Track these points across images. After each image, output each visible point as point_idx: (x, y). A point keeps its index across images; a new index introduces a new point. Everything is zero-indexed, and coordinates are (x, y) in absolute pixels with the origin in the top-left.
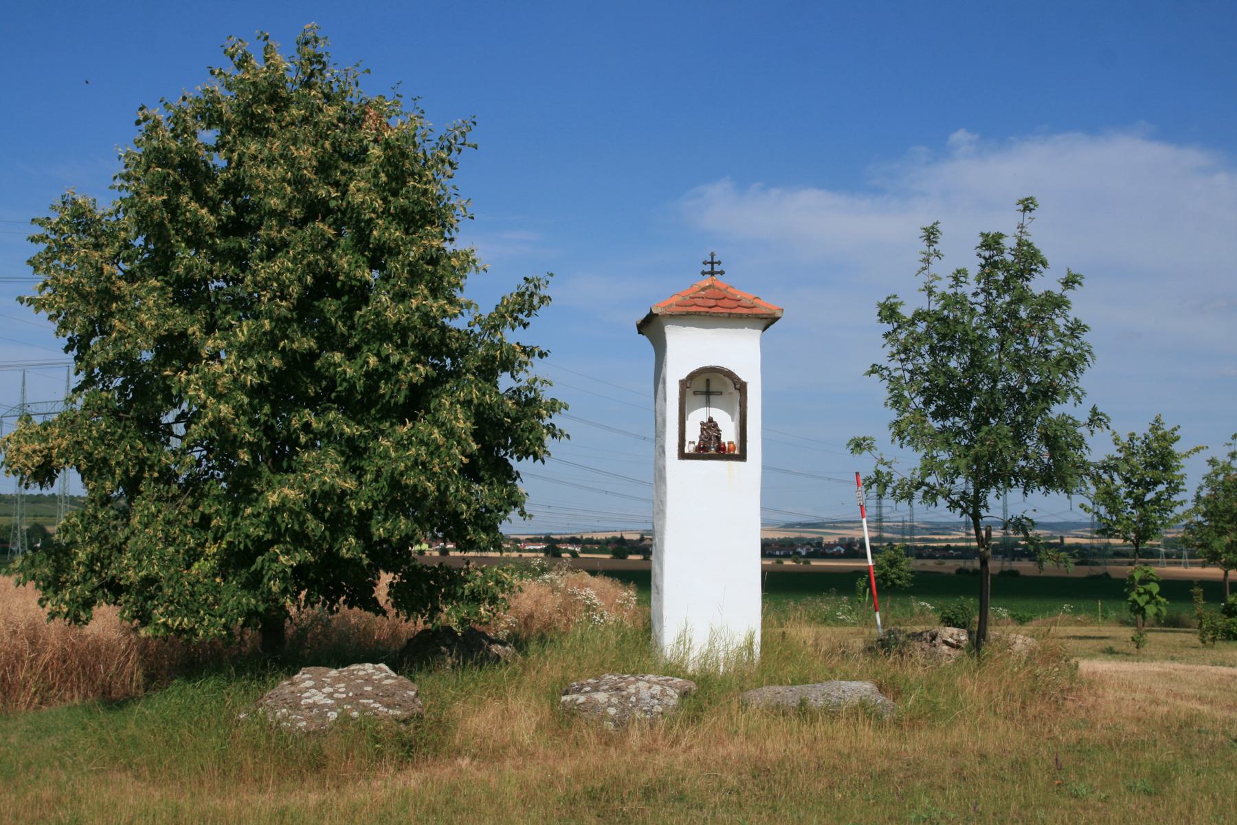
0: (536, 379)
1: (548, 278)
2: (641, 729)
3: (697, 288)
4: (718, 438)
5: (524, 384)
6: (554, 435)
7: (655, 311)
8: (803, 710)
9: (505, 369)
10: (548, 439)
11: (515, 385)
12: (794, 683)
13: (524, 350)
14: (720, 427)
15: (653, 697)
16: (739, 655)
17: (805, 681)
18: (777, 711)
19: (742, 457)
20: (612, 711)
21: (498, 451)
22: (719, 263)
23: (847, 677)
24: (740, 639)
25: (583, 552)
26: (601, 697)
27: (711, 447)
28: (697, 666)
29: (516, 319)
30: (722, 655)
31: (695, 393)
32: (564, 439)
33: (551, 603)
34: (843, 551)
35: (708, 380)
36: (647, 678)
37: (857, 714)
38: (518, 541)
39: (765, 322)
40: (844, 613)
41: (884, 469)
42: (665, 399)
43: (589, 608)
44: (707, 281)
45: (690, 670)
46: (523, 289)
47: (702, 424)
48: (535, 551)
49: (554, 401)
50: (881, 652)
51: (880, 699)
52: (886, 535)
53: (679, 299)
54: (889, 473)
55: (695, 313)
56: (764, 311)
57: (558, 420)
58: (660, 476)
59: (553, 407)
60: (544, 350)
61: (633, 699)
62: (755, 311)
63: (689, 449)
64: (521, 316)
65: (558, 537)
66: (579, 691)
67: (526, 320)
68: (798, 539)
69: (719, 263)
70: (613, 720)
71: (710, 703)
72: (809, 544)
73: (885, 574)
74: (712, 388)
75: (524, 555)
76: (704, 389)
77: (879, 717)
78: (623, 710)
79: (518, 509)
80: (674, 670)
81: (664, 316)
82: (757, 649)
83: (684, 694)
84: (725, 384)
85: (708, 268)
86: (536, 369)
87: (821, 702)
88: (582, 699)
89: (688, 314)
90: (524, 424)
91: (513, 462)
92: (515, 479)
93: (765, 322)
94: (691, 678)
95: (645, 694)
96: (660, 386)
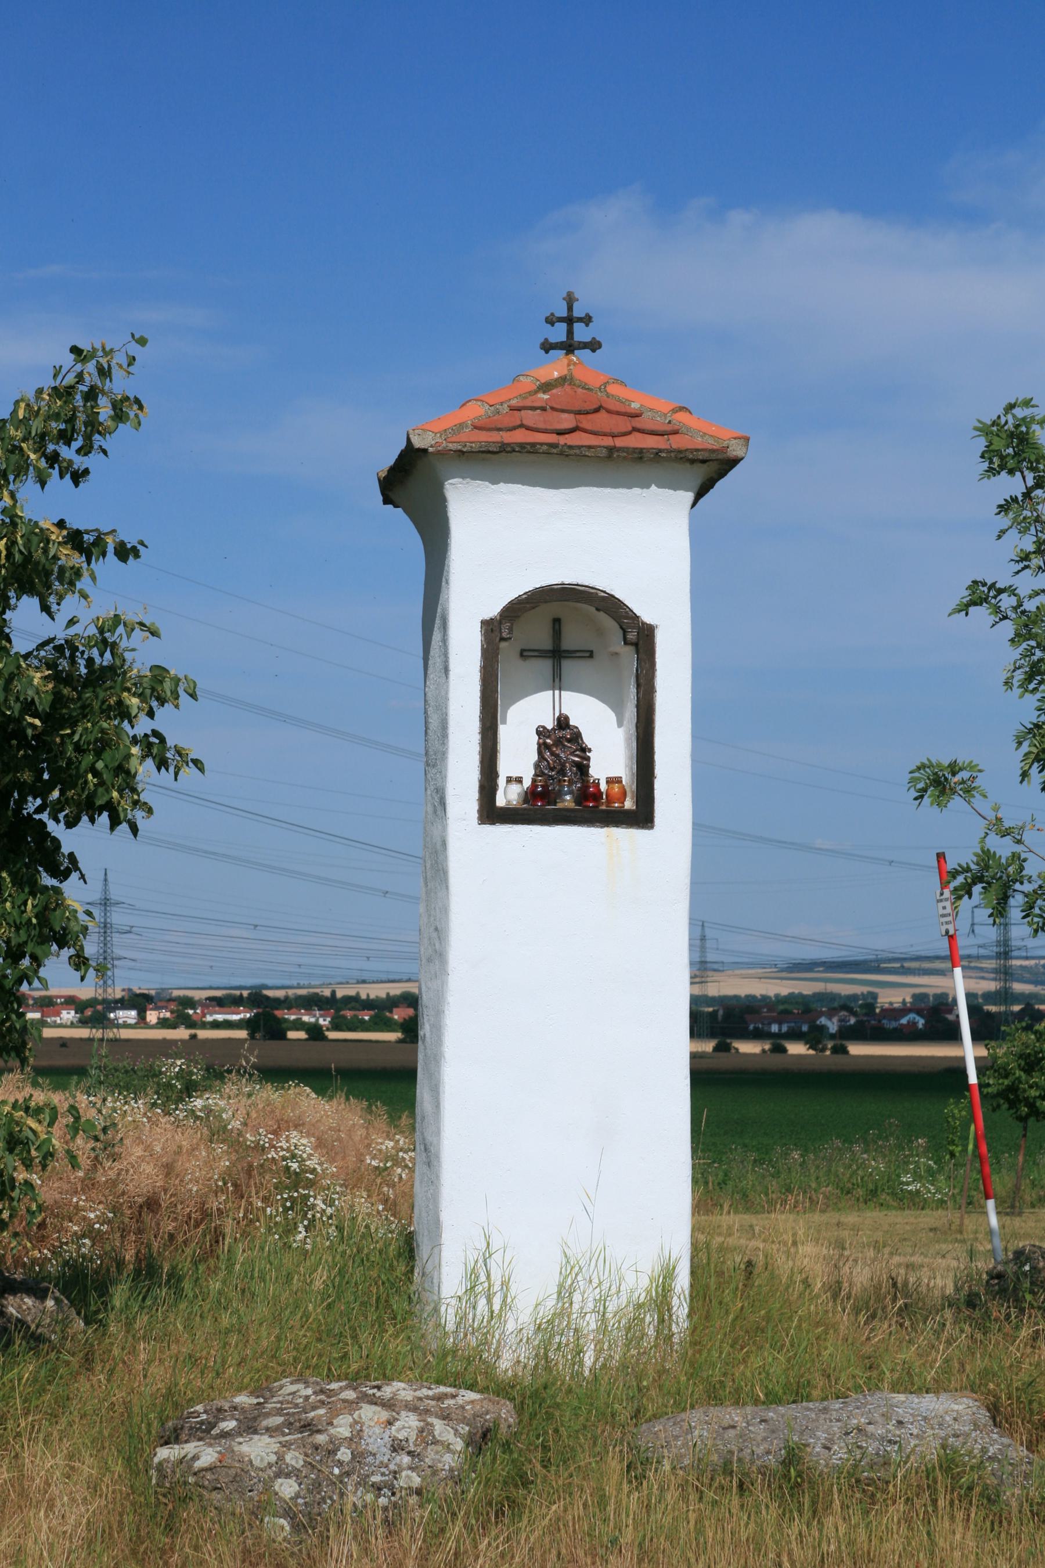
0: (117, 620)
1: (134, 349)
2: (362, 1537)
3: (527, 383)
4: (583, 769)
5: (86, 629)
6: (162, 763)
7: (418, 443)
8: (793, 1478)
9: (26, 588)
10: (145, 771)
11: (57, 630)
12: (773, 1399)
13: (75, 539)
14: (588, 740)
15: (397, 1447)
16: (633, 1330)
17: (798, 1393)
18: (727, 1477)
19: (642, 816)
20: (287, 1488)
21: (22, 802)
22: (587, 320)
23: (908, 1383)
24: (637, 1282)
25: (336, 1026)
26: (258, 1450)
27: (563, 793)
28: (524, 1354)
29: (53, 459)
30: (591, 1322)
31: (523, 654)
32: (189, 772)
33: (203, 1168)
34: (921, 1022)
35: (557, 622)
36: (387, 1391)
37: (932, 1489)
38: (189, 1003)
39: (699, 474)
40: (917, 1177)
41: (1003, 848)
42: (446, 670)
43: (297, 1180)
44: (556, 366)
45: (505, 1363)
46: (70, 380)
47: (541, 732)
48: (228, 1025)
49: (159, 673)
50: (997, 1309)
51: (995, 1442)
52: (1018, 987)
53: (476, 411)
54: (1015, 856)
55: (530, 449)
56: (699, 442)
57: (169, 722)
58: (433, 865)
59: (159, 688)
60: (131, 541)
61: (344, 1454)
62: (676, 442)
63: (507, 796)
64: (67, 453)
65: (280, 994)
66: (204, 1431)
67: (80, 462)
68: (819, 997)
69: (587, 320)
70: (288, 1513)
71: (546, 1464)
72: (845, 1007)
73: (1013, 1089)
74: (567, 644)
75: (203, 1034)
76: (547, 644)
77: (991, 1498)
78: (317, 1485)
79: (67, 952)
80: (462, 1367)
81: (442, 454)
82: (681, 1309)
83: (481, 1439)
84: (600, 632)
85: (559, 334)
86: (102, 594)
87: (840, 1453)
88: (208, 1456)
89: (505, 449)
90: (83, 731)
91: (56, 829)
92: (64, 875)
93: (699, 474)
94: (503, 1389)
95: (376, 1440)
96: (437, 636)
